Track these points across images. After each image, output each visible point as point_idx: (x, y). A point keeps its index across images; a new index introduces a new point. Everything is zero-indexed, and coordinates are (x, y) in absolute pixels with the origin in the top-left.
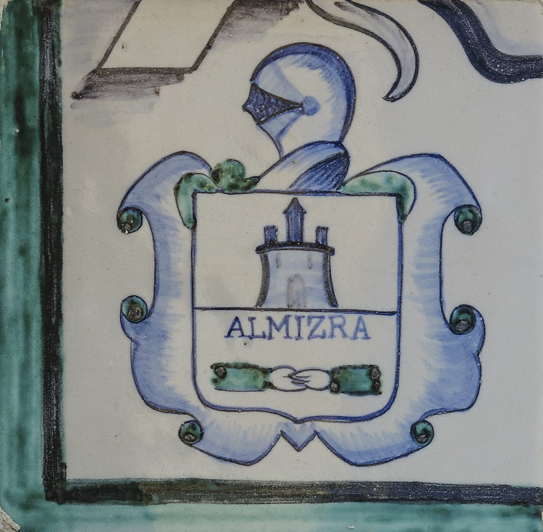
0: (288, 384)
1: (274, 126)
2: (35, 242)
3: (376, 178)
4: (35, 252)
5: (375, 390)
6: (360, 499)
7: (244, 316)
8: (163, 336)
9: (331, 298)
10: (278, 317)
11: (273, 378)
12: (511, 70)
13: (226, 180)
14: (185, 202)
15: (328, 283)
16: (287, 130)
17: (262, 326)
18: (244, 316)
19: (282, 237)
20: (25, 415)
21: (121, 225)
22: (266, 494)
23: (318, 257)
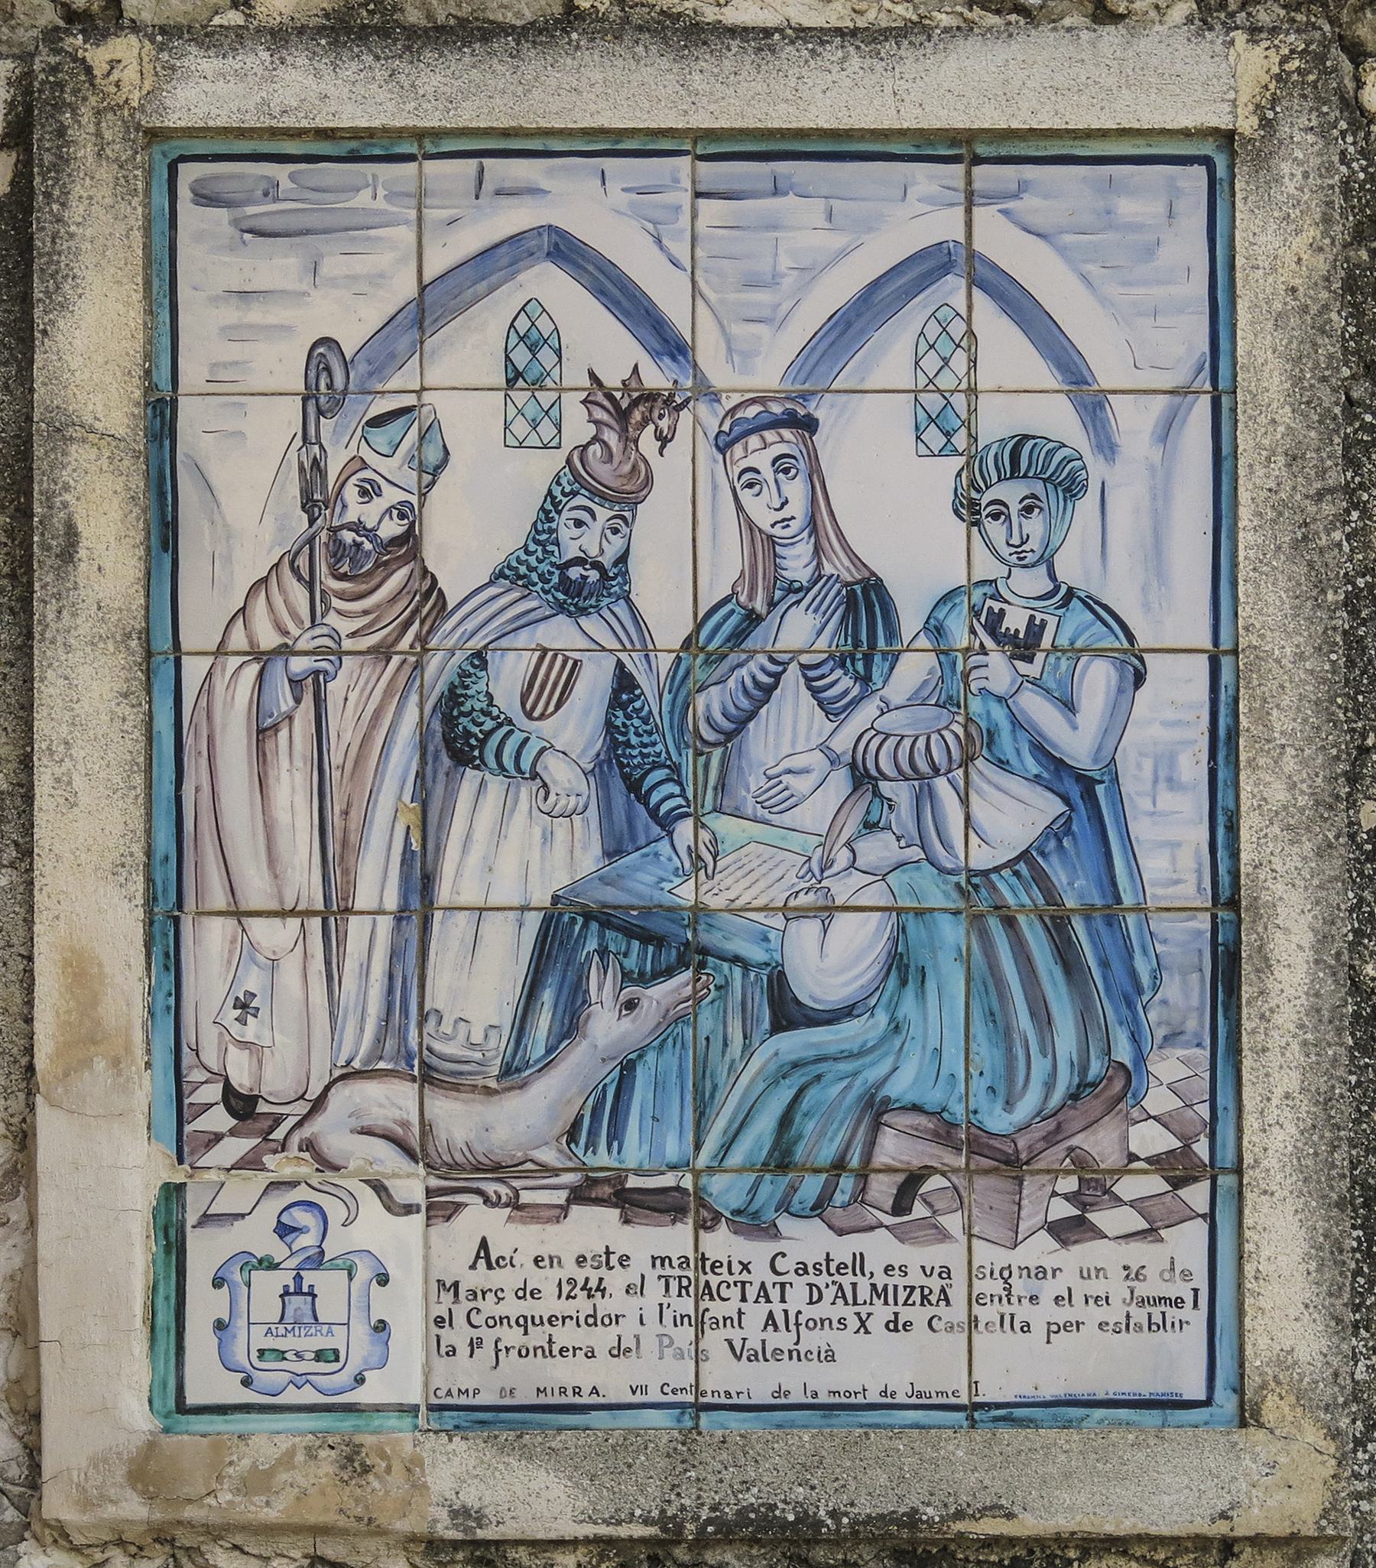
0: (294, 1358)
1: (288, 1239)
2: (173, 1294)
3: (339, 1262)
4: (173, 1301)
5: (337, 1360)
6: (330, 1411)
7: (273, 1327)
8: (235, 1337)
9: (316, 1319)
10: (290, 1327)
11: (287, 1355)
12: (1360, 725)
13: (265, 1264)
14: (246, 1274)
15: (314, 1311)
16: (381, 1132)
17: (282, 1331)
18: (273, 1327)
19: (292, 1290)
20: (166, 1374)
21: (214, 1286)
22: (39, 140)
23: (309, 1299)
